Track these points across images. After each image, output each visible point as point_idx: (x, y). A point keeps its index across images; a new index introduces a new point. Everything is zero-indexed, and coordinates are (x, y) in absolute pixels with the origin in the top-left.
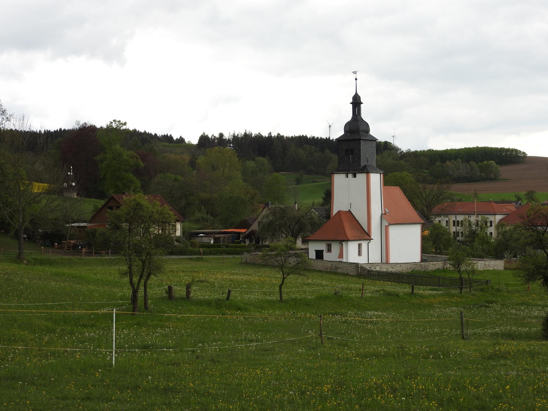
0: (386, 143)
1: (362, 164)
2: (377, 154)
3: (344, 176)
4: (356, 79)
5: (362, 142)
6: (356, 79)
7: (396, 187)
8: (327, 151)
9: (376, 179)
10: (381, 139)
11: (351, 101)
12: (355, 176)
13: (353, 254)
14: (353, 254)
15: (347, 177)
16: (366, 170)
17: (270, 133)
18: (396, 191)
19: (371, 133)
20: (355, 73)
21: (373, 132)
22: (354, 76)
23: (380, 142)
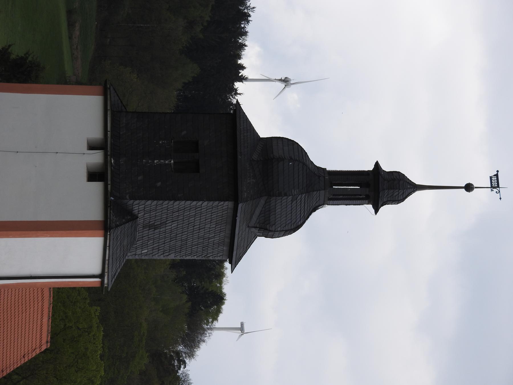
0: (219, 299)
1: (140, 207)
2: (174, 265)
3: (96, 132)
4: (469, 188)
5: (228, 205)
6: (469, 188)
7: (45, 337)
8: (192, 70)
9: (81, 257)
10: (234, 282)
11: (386, 167)
12: (93, 176)
13: (227, 265)
14: (227, 265)
15: (92, 147)
16: (114, 221)
17: (376, 212)
18: (31, 337)
19: (261, 244)
20: (495, 183)
21: (265, 253)
22: (481, 180)
23: (220, 276)
